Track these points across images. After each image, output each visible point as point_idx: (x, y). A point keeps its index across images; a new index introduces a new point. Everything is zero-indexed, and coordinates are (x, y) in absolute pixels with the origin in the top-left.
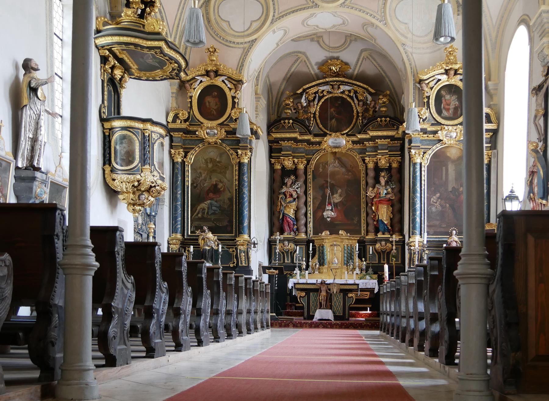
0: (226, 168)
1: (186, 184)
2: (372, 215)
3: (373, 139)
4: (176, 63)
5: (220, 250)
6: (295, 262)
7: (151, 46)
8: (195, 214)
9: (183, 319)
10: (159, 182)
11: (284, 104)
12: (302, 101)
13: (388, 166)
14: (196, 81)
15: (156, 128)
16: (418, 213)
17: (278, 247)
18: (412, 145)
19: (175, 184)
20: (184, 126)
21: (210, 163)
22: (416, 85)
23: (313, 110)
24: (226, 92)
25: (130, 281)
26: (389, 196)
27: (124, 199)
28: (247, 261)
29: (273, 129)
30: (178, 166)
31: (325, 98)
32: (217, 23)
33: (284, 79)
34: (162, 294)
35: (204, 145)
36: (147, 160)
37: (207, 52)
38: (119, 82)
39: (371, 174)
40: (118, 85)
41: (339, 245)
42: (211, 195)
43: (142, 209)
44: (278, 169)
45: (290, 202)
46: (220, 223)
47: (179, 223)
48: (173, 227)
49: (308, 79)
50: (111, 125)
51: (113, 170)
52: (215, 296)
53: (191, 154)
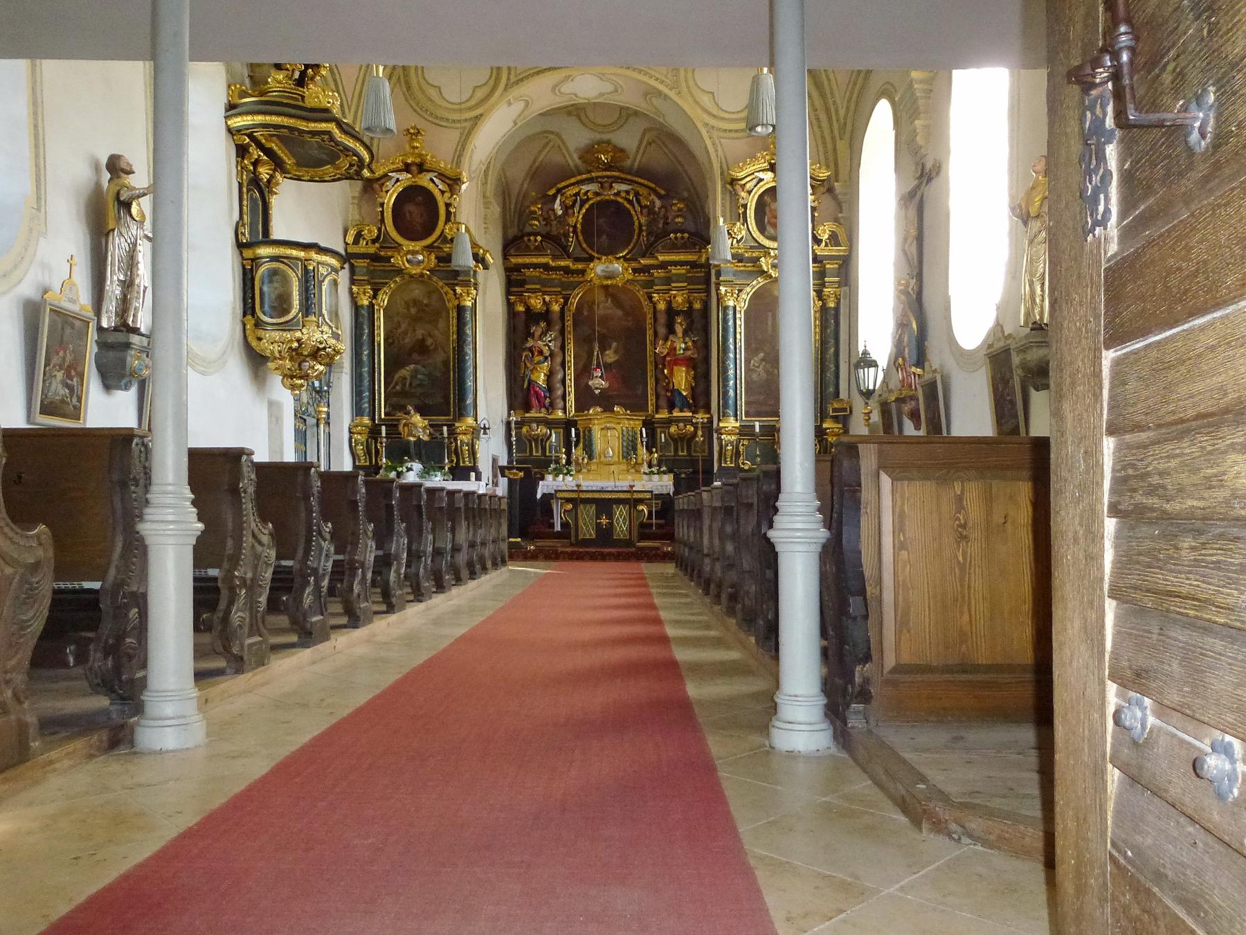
2: (663, 383)
3: (663, 265)
6: (548, 454)
8: (392, 386)
9: (360, 577)
10: (332, 342)
12: (556, 206)
16: (731, 383)
18: (721, 278)
20: (372, 250)
22: (726, 187)
23: (572, 221)
25: (266, 532)
26: (689, 353)
27: (276, 369)
30: (363, 312)
31: (591, 202)
32: (421, 89)
33: (527, 174)
34: (323, 543)
39: (662, 319)
41: (614, 428)
42: (415, 356)
45: (539, 363)
47: (366, 400)
49: (565, 173)
51: (258, 324)
52: (414, 534)
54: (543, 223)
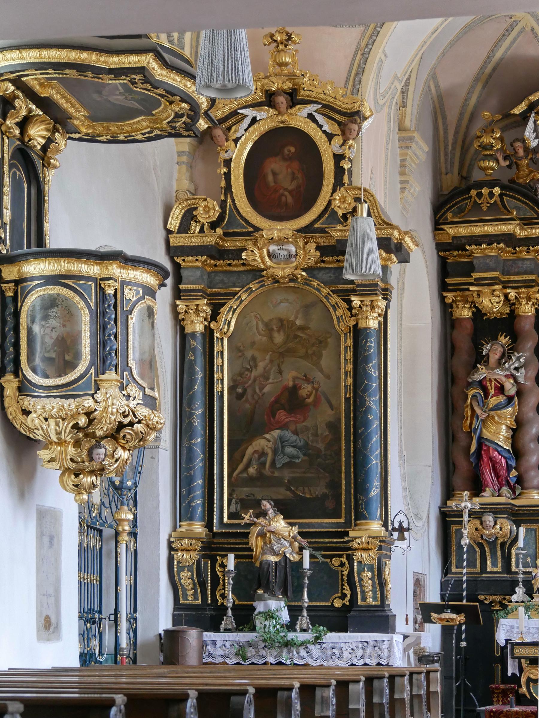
0: (321, 343)
1: (217, 387)
4: (183, 101)
5: (306, 564)
6: (514, 569)
7: (120, 66)
8: (241, 467)
10: (143, 412)
11: (476, 145)
12: (527, 134)
13: (507, 314)
14: (242, 119)
15: (134, 272)
17: (465, 532)
19: (188, 391)
21: (279, 331)
24: (319, 144)
27: (52, 460)
28: (378, 593)
29: (449, 215)
33: (477, 79)
35: (261, 286)
36: (112, 357)
37: (270, 44)
38: (41, 153)
40: (38, 162)
42: (282, 415)
43: (99, 482)
44: (464, 319)
45: (497, 408)
46: (306, 490)
48: (183, 505)
50: (19, 271)
53: (229, 311)
54: (504, 164)
